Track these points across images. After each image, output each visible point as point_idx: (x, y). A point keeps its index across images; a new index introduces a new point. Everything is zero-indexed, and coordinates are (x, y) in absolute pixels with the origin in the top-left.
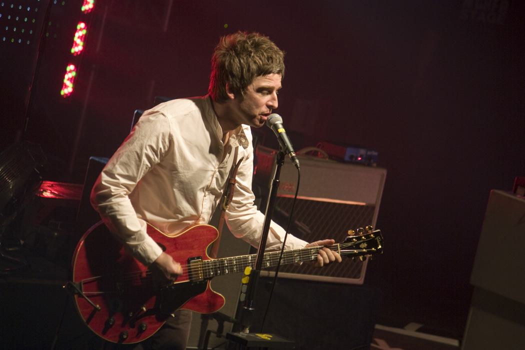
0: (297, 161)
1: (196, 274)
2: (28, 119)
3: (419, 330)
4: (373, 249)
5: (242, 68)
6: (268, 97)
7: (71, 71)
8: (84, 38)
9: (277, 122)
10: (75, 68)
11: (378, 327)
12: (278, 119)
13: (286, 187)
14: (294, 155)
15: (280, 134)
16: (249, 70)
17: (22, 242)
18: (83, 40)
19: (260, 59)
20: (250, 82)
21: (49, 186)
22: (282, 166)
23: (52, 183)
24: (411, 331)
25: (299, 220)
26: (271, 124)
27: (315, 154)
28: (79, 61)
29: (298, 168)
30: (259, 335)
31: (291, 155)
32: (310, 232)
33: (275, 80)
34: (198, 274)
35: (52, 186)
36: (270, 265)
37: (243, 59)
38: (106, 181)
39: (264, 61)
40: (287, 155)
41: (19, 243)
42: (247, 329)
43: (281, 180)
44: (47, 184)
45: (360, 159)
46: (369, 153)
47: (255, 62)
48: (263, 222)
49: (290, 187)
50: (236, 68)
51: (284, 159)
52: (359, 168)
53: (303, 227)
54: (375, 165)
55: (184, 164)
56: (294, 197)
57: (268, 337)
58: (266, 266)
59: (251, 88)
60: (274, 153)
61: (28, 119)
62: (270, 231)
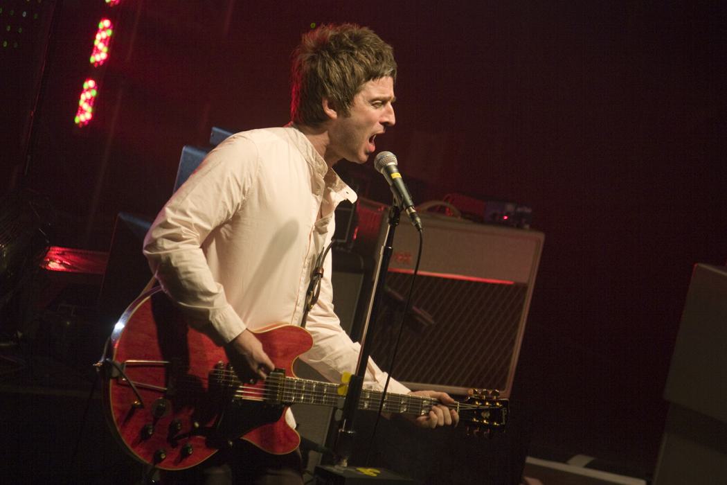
0: (418, 220)
1: (274, 384)
2: (29, 157)
3: (589, 466)
4: (495, 424)
5: (343, 73)
6: (383, 109)
7: (89, 91)
8: (110, 42)
9: (390, 164)
10: (95, 85)
11: (530, 460)
12: (390, 159)
13: (400, 257)
14: (414, 211)
15: (394, 181)
16: (353, 73)
17: (20, 334)
18: (91, 104)
19: (366, 57)
20: (356, 90)
21: (58, 254)
22: (396, 228)
23: (64, 249)
24: (577, 467)
25: (418, 307)
26: (381, 167)
27: (442, 210)
28: (103, 74)
29: (419, 230)
30: (361, 470)
31: (410, 211)
32: (433, 322)
33: (384, 87)
34: (277, 393)
35: (63, 254)
36: (369, 407)
37: (343, 59)
38: (173, 219)
39: (372, 59)
40: (402, 212)
41: (15, 335)
42: (345, 461)
43: (395, 247)
44: (55, 250)
45: (506, 218)
46: (519, 210)
47: (361, 63)
48: (357, 360)
49: (405, 258)
50: (335, 75)
51: (399, 217)
52: (504, 230)
53: (423, 314)
54: (527, 226)
55: (259, 220)
56: (413, 272)
57: (375, 473)
58: (363, 406)
59: (360, 99)
60: (383, 209)
61: (29, 157)
62: (367, 369)
